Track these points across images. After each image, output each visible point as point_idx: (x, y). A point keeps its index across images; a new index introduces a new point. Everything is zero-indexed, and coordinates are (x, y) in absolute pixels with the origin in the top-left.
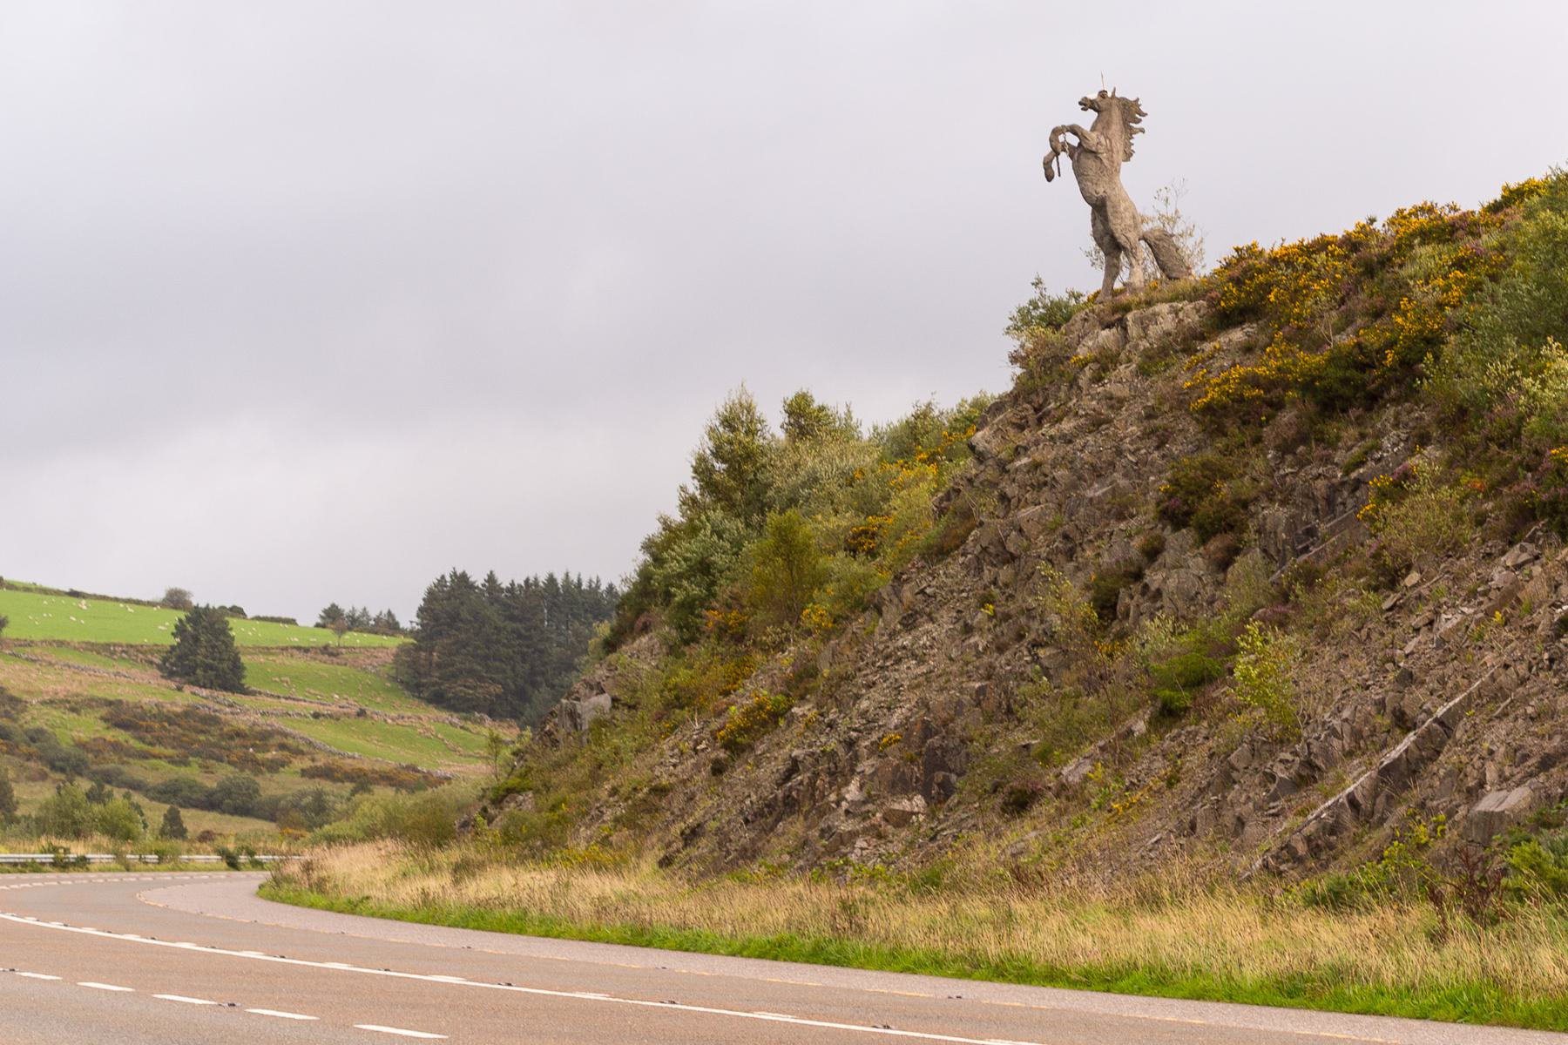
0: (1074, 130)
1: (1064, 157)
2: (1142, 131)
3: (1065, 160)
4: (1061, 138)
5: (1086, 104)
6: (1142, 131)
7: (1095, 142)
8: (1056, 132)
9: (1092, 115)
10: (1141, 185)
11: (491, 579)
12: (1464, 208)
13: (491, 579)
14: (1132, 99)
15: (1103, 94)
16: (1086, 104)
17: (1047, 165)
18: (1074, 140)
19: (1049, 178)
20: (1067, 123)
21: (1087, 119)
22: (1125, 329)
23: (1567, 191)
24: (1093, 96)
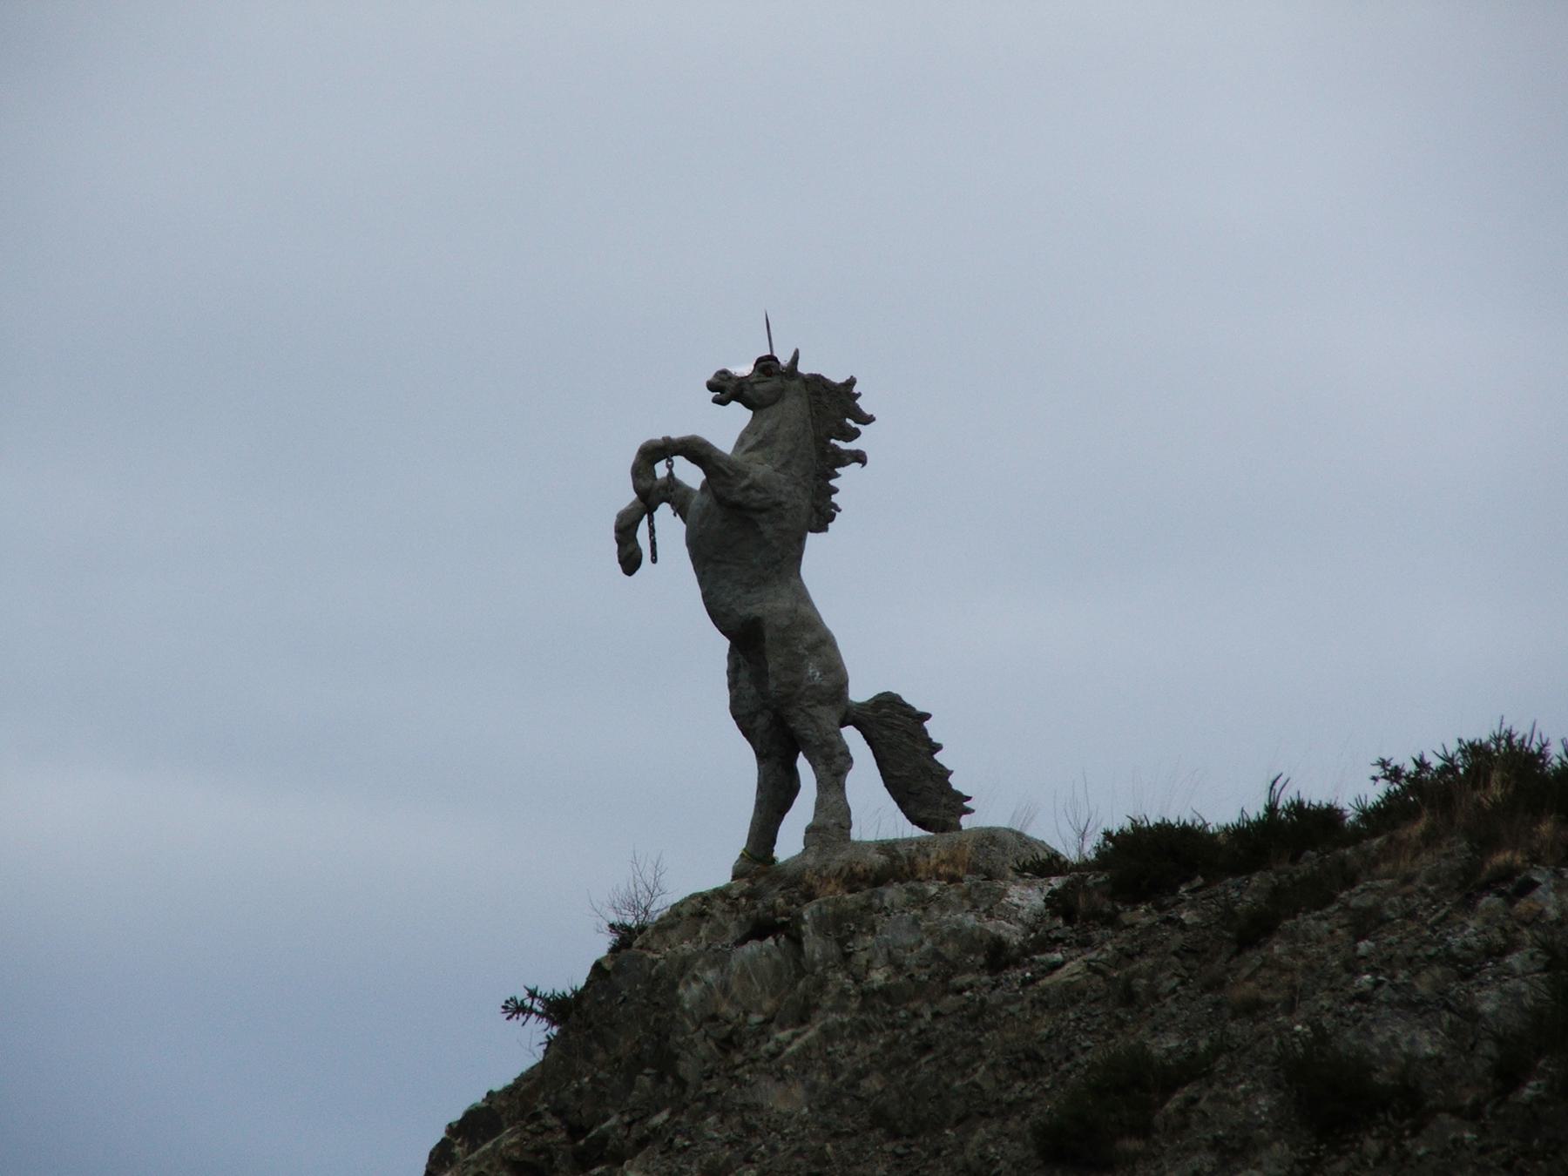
0: (695, 450)
1: (664, 512)
2: (860, 457)
3: (669, 526)
4: (661, 470)
5: (725, 388)
6: (860, 457)
7: (754, 491)
8: (653, 453)
9: (738, 416)
10: (866, 591)
11: (859, 395)
12: (559, 991)
13: (859, 395)
14: (838, 378)
15: (766, 365)
16: (725, 388)
17: (625, 531)
18: (690, 475)
19: (630, 563)
20: (677, 434)
21: (726, 427)
22: (796, 940)
23: (1511, 811)
24: (744, 369)
